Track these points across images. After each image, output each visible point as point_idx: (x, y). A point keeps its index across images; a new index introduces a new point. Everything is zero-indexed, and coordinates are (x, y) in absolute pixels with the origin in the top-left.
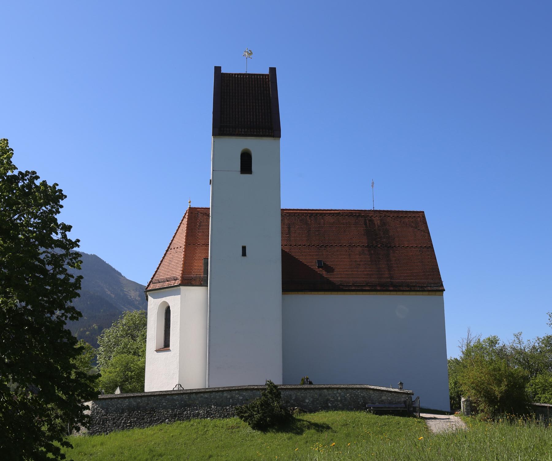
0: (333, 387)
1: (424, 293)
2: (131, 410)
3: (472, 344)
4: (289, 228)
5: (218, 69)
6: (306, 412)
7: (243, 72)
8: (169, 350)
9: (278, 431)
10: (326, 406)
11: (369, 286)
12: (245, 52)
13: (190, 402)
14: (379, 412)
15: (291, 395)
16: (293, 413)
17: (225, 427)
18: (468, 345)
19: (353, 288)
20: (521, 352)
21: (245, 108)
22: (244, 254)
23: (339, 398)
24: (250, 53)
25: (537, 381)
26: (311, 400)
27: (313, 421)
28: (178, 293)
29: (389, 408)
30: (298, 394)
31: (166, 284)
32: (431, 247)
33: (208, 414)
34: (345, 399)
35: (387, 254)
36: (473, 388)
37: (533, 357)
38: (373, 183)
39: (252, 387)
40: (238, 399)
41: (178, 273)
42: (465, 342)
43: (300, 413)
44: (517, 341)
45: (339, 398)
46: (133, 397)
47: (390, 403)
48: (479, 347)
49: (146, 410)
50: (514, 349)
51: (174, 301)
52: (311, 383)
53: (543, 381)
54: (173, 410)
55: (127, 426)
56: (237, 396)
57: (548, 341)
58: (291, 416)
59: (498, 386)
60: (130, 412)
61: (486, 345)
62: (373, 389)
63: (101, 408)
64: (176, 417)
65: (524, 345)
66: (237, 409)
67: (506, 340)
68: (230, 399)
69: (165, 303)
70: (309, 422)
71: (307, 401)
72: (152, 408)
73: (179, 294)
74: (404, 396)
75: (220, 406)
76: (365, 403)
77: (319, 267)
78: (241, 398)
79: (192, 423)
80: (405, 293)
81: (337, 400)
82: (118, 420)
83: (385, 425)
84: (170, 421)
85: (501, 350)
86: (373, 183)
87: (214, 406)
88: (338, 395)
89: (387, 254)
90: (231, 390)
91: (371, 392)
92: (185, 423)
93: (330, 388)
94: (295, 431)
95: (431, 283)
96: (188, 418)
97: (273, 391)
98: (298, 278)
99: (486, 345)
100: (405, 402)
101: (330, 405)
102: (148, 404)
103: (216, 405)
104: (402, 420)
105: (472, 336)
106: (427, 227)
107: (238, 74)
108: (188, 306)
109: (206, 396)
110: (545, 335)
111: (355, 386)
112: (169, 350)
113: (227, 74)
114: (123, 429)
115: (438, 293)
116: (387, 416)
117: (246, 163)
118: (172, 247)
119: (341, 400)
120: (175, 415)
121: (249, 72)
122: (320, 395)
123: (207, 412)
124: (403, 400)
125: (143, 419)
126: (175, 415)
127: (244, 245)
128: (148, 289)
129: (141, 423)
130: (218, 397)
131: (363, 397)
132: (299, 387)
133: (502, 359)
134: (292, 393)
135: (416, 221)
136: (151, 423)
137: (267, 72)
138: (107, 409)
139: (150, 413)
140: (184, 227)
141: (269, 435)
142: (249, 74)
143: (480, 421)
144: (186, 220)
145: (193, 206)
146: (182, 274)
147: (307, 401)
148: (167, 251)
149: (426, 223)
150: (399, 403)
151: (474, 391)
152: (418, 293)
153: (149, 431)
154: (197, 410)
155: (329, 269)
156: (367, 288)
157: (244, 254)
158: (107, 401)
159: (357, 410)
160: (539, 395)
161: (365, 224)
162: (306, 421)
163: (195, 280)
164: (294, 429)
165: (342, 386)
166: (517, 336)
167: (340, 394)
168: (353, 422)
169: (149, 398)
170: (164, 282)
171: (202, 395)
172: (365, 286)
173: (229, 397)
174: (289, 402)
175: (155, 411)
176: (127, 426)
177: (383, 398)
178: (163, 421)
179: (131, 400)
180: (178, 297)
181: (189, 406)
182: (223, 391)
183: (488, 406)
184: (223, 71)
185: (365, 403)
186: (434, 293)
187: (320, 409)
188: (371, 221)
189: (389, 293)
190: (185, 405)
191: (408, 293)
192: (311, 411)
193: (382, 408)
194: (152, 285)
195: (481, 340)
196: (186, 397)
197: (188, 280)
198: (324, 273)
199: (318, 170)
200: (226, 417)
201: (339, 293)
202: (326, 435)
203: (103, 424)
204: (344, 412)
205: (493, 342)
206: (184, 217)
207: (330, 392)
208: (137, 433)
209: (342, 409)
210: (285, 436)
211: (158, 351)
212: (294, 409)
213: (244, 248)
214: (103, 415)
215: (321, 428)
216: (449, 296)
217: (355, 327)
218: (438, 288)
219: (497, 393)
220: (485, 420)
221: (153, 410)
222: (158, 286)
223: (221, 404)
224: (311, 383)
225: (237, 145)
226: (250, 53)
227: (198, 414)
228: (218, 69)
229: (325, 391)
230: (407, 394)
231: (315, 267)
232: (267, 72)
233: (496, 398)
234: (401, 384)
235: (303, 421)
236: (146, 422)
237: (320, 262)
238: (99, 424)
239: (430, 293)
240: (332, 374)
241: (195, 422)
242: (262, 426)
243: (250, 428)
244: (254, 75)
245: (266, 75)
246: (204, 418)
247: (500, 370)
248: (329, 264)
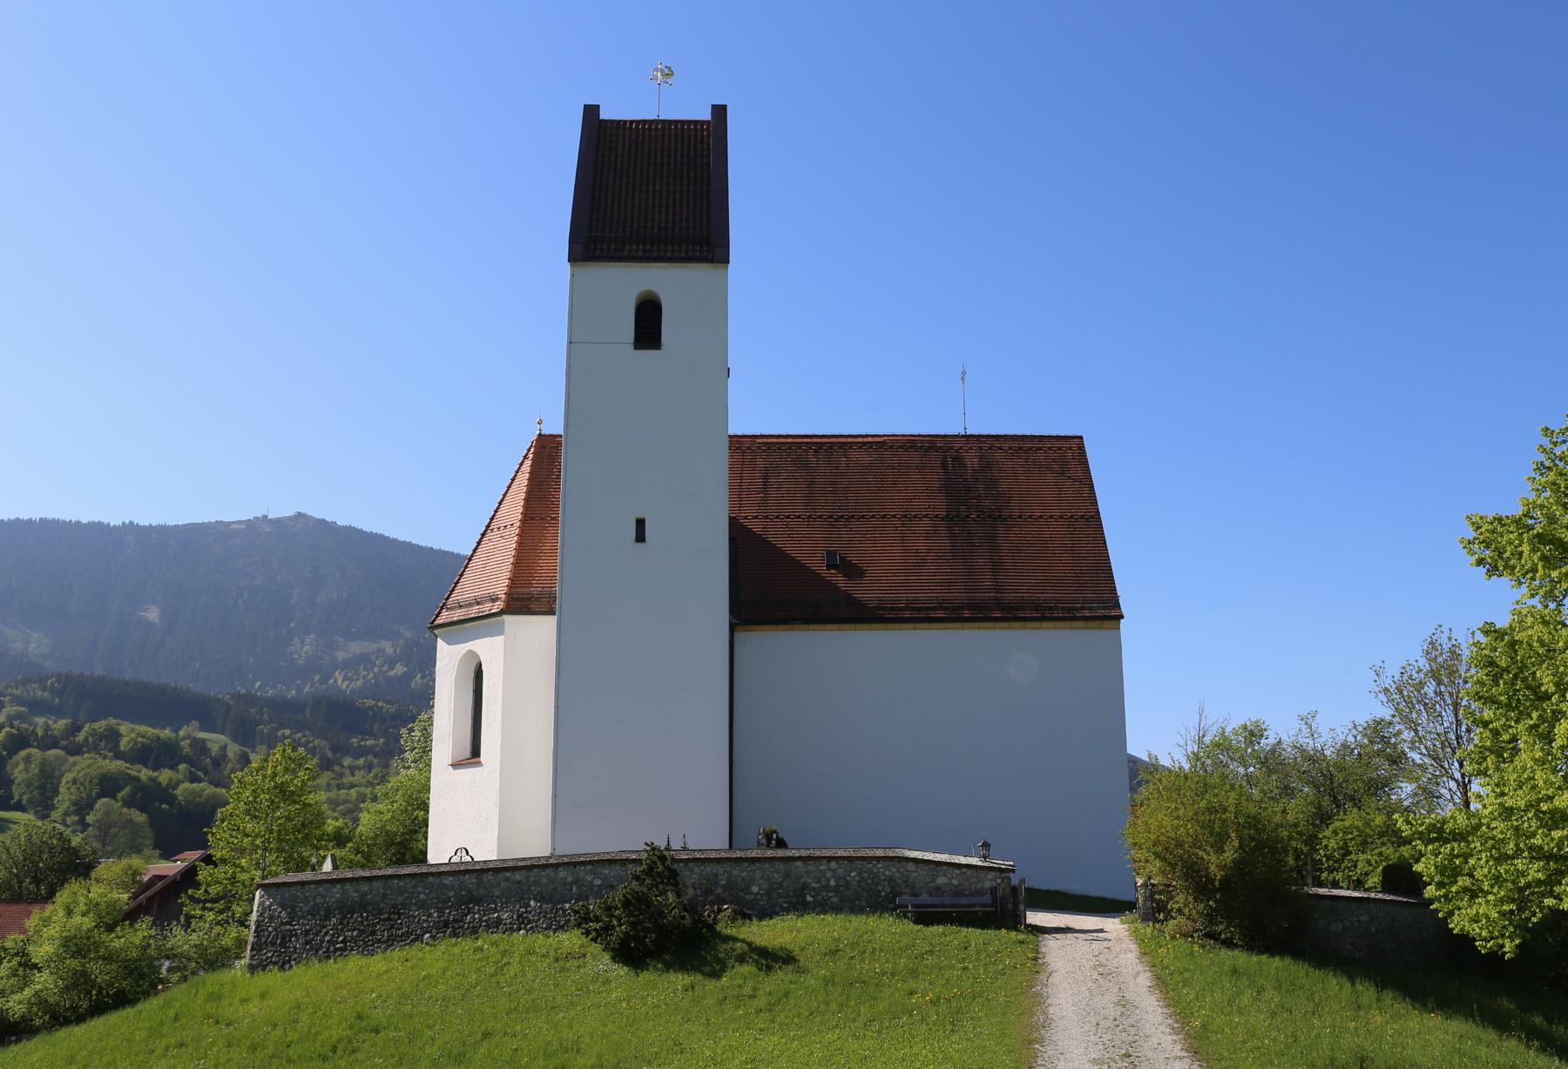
0: (818, 854)
1: (1075, 624)
2: (346, 910)
3: (1207, 740)
4: (766, 478)
5: (591, 112)
6: (750, 917)
7: (652, 116)
8: (479, 764)
9: (668, 967)
10: (799, 903)
11: (946, 609)
12: (656, 69)
13: (482, 892)
14: (925, 917)
15: (716, 875)
16: (715, 921)
17: (552, 954)
18: (1200, 741)
19: (907, 614)
20: (1314, 758)
21: (650, 197)
22: (640, 537)
23: (832, 883)
24: (669, 73)
25: (1347, 823)
26: (766, 886)
27: (758, 941)
28: (499, 631)
29: (952, 906)
30: (735, 873)
31: (474, 611)
32: (1096, 517)
33: (522, 922)
34: (847, 885)
35: (997, 535)
36: (1157, 856)
37: (1341, 768)
38: (964, 373)
39: (624, 856)
40: (592, 884)
41: (500, 586)
42: (1194, 733)
43: (733, 920)
44: (1306, 731)
45: (832, 883)
46: (352, 880)
47: (958, 893)
48: (1222, 745)
49: (380, 912)
50: (1302, 750)
51: (490, 649)
52: (781, 844)
53: (1360, 824)
54: (441, 911)
55: (336, 950)
56: (589, 878)
57: (1375, 730)
58: (711, 928)
59: (1216, 852)
60: (344, 917)
61: (1239, 741)
62: (915, 860)
63: (280, 905)
64: (451, 928)
65: (1322, 740)
66: (576, 912)
67: (1283, 730)
68: (572, 884)
69: (472, 654)
70: (749, 944)
71: (755, 889)
72: (395, 906)
73: (500, 633)
74: (991, 875)
75: (549, 901)
76: (895, 894)
77: (829, 567)
78: (598, 882)
79: (479, 943)
80: (1028, 624)
81: (827, 888)
82: (317, 934)
83: (931, 952)
84: (433, 937)
85: (1273, 751)
86: (964, 373)
87: (536, 901)
88: (829, 874)
89: (997, 535)
90: (575, 864)
91: (911, 866)
92: (465, 945)
93: (809, 858)
94: (708, 969)
95: (1092, 601)
96: (474, 931)
97: (661, 867)
98: (771, 588)
99: (1239, 741)
100: (994, 890)
101: (809, 898)
102: (385, 896)
103: (541, 899)
104: (974, 935)
105: (1210, 722)
106: (1088, 471)
107: (638, 122)
108: (515, 662)
109: (518, 876)
110: (1369, 718)
111: (870, 853)
112: (479, 764)
113: (612, 122)
114: (328, 957)
115: (1107, 623)
116: (941, 929)
117: (648, 325)
118: (494, 525)
119: (837, 886)
120: (446, 924)
121: (667, 115)
122: (787, 875)
123: (519, 916)
124: (988, 884)
125: (373, 933)
126: (446, 924)
127: (641, 516)
128: (440, 621)
129: (367, 942)
130: (544, 881)
131: (891, 880)
132: (754, 854)
133: (1270, 772)
134: (718, 869)
135: (1064, 457)
136: (389, 943)
137: (706, 115)
138: (293, 908)
139: (389, 919)
140: (523, 479)
141: (646, 976)
142: (664, 121)
143: (1173, 938)
144: (528, 463)
145: (546, 431)
146: (510, 587)
147: (755, 889)
148: (483, 535)
149: (1086, 463)
150: (979, 892)
151: (1158, 863)
152: (1059, 624)
153: (377, 963)
154: (495, 910)
155: (853, 571)
156: (940, 614)
157: (640, 537)
158: (293, 891)
159: (874, 912)
160: (1353, 857)
161: (944, 466)
162: (743, 941)
163: (537, 600)
164: (706, 963)
165: (841, 853)
166: (1307, 721)
167: (834, 871)
168: (853, 945)
169: (389, 882)
170: (470, 605)
171: (508, 874)
172: (934, 609)
173: (570, 879)
174: (712, 892)
175: (400, 915)
176: (336, 950)
177: (941, 881)
178: (419, 938)
179: (348, 886)
180: (499, 640)
181: (478, 901)
182: (556, 866)
183: (1195, 899)
184: (604, 115)
185: (895, 894)
186: (1097, 623)
187: (783, 909)
188: (958, 459)
189: (991, 624)
190: (470, 900)
191: (1036, 624)
192: (764, 915)
193: (936, 906)
194: (444, 613)
195: (1228, 730)
196: (470, 880)
197: (525, 598)
198: (841, 581)
199: (817, 342)
200: (562, 927)
201: (874, 626)
202: (781, 977)
203: (282, 945)
204: (840, 917)
205: (1253, 734)
206: (525, 457)
207: (811, 867)
208: (353, 967)
209: (837, 909)
210: (680, 979)
211: (455, 765)
212: (720, 910)
213: (640, 524)
214: (282, 924)
215: (770, 959)
216: (1137, 632)
217: (903, 706)
218: (1106, 613)
219: (1213, 868)
220: (1185, 935)
221: (396, 910)
222: (457, 615)
223: (551, 898)
224: (781, 844)
225: (628, 281)
226: (669, 73)
227: (499, 921)
228: (591, 112)
229: (799, 863)
230: (1000, 870)
231: (821, 568)
232: (706, 115)
233: (1212, 881)
234: (986, 845)
235: (735, 940)
236: (379, 941)
237: (831, 555)
238: (273, 944)
239: (1089, 624)
240: (838, 821)
241: (484, 941)
242: (631, 955)
243: (606, 957)
244: (677, 122)
245: (702, 122)
246: (512, 930)
247: (1225, 810)
248: (853, 558)
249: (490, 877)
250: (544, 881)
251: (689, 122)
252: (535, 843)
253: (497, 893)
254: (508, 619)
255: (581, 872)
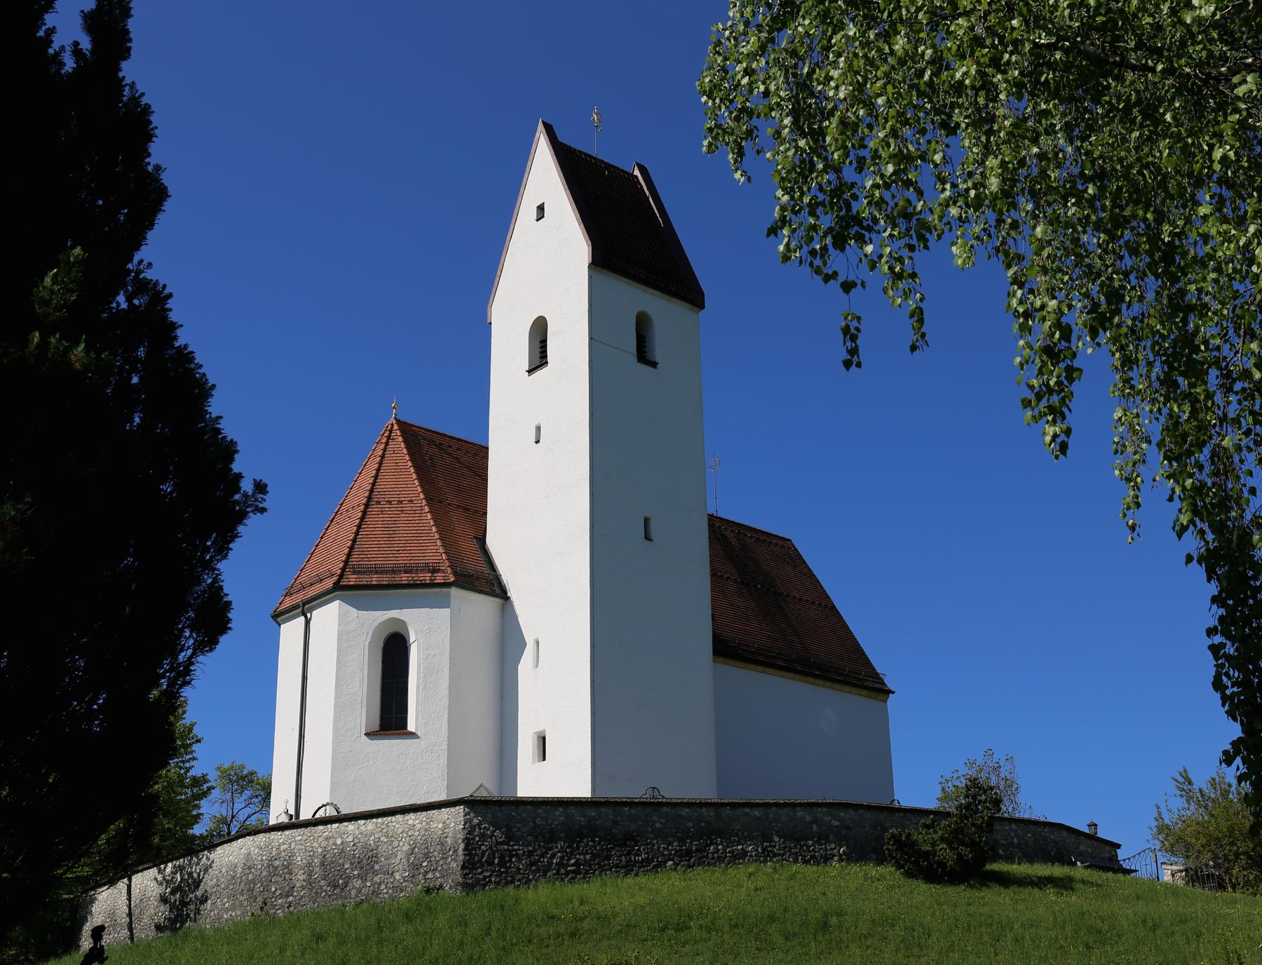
28: (445, 604)
33: (766, 855)
45: (1015, 841)
63: (491, 824)
82: (543, 855)
87: (780, 837)
101: (1001, 852)
102: (615, 822)
120: (689, 853)
123: (764, 849)
125: (608, 858)
126: (689, 853)
137: (411, 727)
138: (509, 828)
171: (747, 810)
173: (808, 819)
176: (567, 873)
181: (720, 834)
190: (710, 833)
203: (502, 863)
227: (744, 853)
249: (727, 811)
250: (784, 818)
251: (608, 166)
252: (583, 790)
253: (738, 827)
254: (455, 592)
255: (820, 812)
